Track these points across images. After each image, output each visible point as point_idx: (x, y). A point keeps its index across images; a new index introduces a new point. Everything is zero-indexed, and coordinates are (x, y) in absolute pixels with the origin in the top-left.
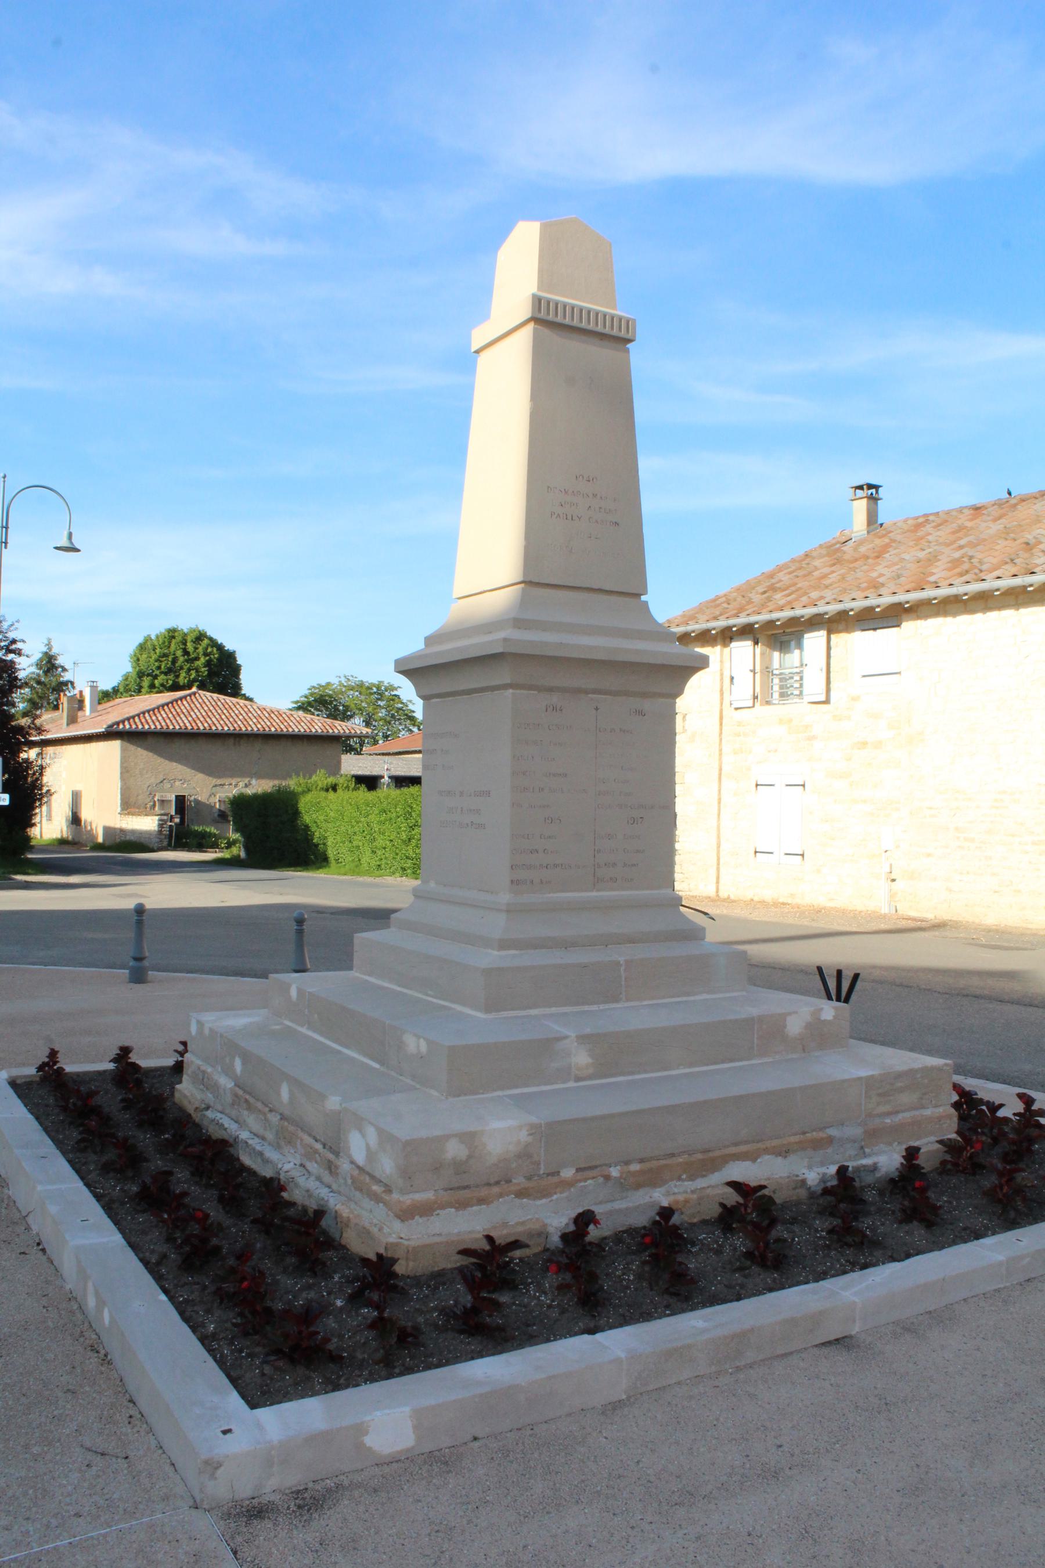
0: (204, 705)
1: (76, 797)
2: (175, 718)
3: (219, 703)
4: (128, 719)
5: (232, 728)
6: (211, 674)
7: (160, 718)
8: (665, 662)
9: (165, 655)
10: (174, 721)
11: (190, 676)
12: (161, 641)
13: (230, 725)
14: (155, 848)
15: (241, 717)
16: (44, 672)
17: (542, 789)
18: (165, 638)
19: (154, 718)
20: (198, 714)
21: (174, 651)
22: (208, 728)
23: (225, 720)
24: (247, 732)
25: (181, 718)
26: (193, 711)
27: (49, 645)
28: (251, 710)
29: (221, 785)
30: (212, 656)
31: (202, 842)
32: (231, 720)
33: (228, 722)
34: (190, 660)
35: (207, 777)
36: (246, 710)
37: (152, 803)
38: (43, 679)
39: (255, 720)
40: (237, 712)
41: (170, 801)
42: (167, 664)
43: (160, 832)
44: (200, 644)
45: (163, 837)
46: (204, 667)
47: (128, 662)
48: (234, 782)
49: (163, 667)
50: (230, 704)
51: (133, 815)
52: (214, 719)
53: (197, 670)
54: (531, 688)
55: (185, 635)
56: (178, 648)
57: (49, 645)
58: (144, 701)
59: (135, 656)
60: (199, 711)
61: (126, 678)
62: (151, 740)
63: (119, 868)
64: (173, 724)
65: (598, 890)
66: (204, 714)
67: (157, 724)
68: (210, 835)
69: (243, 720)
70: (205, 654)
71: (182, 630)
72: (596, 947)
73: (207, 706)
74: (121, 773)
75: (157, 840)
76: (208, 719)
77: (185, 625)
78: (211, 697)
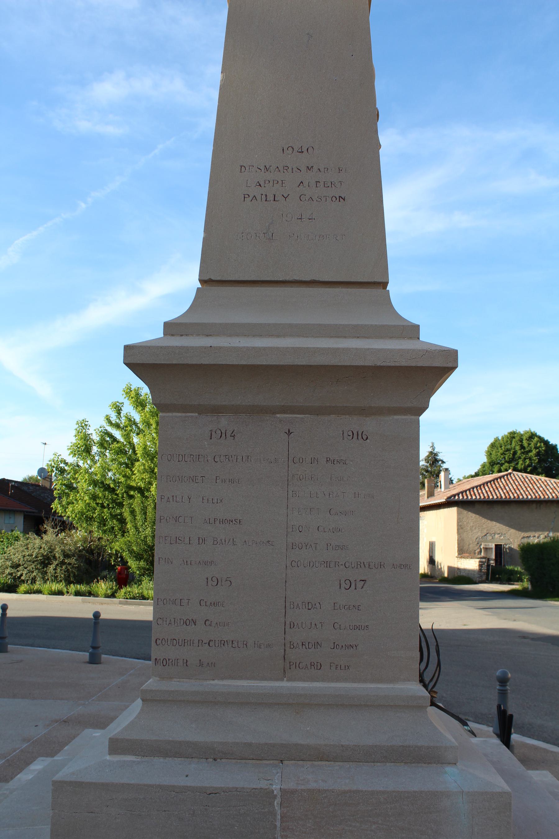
0: (516, 482)
1: (432, 546)
2: (494, 491)
3: (527, 480)
4: (462, 493)
5: (534, 497)
6: (540, 461)
7: (484, 491)
8: (379, 364)
9: (508, 450)
10: (493, 493)
11: (525, 463)
12: (505, 439)
13: (532, 495)
14: (477, 582)
15: (541, 489)
16: (430, 464)
17: (204, 540)
18: (508, 438)
19: (480, 491)
20: (511, 487)
21: (515, 447)
22: (517, 497)
23: (530, 491)
24: (545, 499)
25: (499, 491)
26: (508, 485)
27: (433, 447)
28: (549, 483)
29: (527, 537)
30: (540, 449)
31: (510, 578)
32: (534, 491)
33: (531, 493)
34: (526, 452)
35: (517, 532)
36: (545, 483)
37: (479, 550)
38: (429, 469)
39: (551, 491)
40: (539, 485)
41: (492, 548)
42: (510, 456)
43: (480, 570)
44: (532, 441)
45: (483, 574)
46: (535, 457)
47: (484, 456)
48: (537, 535)
49: (506, 458)
50: (535, 480)
51: (464, 558)
52: (522, 491)
53: (530, 459)
54: (185, 408)
55: (522, 435)
56: (517, 444)
57: (433, 447)
58: (479, 480)
59: (489, 452)
60: (512, 485)
61: (483, 466)
62: (477, 506)
64: (492, 495)
66: (515, 487)
67: (481, 495)
68: (517, 572)
69: (542, 491)
70: (536, 448)
71: (520, 432)
73: (518, 482)
74: (458, 529)
75: (479, 576)
76: (517, 491)
77: (521, 429)
78: (522, 475)
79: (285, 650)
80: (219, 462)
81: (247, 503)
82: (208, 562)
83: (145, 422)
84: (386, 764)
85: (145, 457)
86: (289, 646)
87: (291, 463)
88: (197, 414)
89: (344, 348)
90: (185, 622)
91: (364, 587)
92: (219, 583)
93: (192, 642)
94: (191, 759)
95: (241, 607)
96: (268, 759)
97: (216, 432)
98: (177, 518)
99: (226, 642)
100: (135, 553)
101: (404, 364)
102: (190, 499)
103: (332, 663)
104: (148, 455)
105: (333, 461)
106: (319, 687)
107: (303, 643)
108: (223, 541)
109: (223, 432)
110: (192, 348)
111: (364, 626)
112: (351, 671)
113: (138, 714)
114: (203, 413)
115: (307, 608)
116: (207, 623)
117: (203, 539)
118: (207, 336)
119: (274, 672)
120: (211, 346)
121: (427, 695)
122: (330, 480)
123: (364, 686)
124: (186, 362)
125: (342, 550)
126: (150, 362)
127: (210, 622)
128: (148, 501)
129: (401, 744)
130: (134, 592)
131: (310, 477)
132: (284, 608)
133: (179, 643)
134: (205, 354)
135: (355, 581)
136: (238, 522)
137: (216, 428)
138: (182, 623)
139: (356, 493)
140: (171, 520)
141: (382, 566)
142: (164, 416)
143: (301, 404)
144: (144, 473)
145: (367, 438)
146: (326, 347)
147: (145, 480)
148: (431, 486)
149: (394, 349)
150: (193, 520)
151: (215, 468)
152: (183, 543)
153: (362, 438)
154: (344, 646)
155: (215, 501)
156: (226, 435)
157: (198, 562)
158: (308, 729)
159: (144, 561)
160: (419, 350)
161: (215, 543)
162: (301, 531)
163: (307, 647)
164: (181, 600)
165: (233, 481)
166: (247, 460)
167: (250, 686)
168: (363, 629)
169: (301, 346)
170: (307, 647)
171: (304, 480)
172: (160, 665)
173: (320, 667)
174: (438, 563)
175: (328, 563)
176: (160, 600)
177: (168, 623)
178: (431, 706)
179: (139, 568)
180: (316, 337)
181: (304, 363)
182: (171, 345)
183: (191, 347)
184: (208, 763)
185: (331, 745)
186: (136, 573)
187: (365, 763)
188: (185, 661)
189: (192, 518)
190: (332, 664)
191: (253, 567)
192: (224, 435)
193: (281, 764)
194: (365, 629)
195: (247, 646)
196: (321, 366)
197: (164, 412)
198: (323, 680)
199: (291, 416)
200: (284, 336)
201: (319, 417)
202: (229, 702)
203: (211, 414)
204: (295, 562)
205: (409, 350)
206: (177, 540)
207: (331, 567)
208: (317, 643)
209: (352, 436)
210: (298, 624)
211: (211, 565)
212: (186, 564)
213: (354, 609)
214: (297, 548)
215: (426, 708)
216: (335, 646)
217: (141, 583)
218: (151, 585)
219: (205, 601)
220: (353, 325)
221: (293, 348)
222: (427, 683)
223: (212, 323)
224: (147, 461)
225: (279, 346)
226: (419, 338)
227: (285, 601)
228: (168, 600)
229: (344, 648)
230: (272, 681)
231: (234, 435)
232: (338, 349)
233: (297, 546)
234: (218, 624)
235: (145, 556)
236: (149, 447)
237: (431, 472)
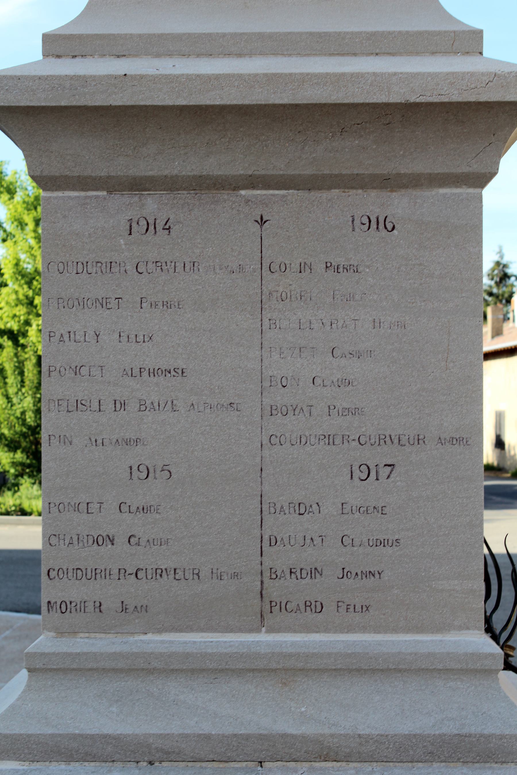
1: (500, 418)
8: (413, 99)
17: (123, 404)
38: (495, 291)
63: (499, 499)
65: (271, 630)
72: (232, 764)
79: (262, 582)
80: (145, 273)
81: (193, 342)
82: (132, 441)
83: (16, 220)
84: (432, 764)
85: (17, 279)
86: (269, 574)
87: (266, 272)
88: (105, 193)
89: (354, 73)
90: (96, 540)
91: (392, 476)
92: (150, 475)
93: (108, 572)
94: (111, 764)
95: (187, 513)
96: (238, 760)
97: (138, 223)
98: (78, 368)
99: (164, 571)
100: (6, 440)
101: (456, 98)
102: (98, 336)
103: (341, 601)
104: (23, 276)
105: (336, 267)
106: (320, 641)
107: (293, 570)
108: (156, 404)
109: (151, 222)
110: (93, 78)
111: (393, 541)
112: (372, 614)
113: (22, 692)
114: (115, 191)
115: (297, 512)
116: (132, 540)
117: (123, 403)
118: (118, 57)
119: (245, 618)
120: (125, 75)
121: (498, 652)
122: (332, 300)
123: (394, 639)
124: (82, 102)
125: (354, 416)
126: (22, 104)
127: (137, 539)
128: (26, 353)
129: (456, 732)
130: (7, 504)
131: (298, 295)
132: (259, 514)
133: (86, 574)
134: (116, 88)
135: (377, 466)
136: (180, 373)
137: (139, 216)
138: (91, 541)
139: (376, 320)
140: (67, 372)
141: (421, 442)
142: (50, 197)
143: (281, 172)
144: (17, 305)
145: (393, 228)
146: (322, 71)
147: (19, 317)
148: (498, 319)
149: (440, 73)
150: (104, 371)
151: (139, 283)
152: (89, 409)
153: (386, 227)
154: (359, 574)
155: (140, 338)
156: (155, 228)
157: (115, 440)
158: (303, 709)
159: (22, 452)
160: (483, 74)
161: (142, 409)
162: (284, 384)
163: (299, 577)
164: (88, 503)
165: (169, 305)
166: (192, 268)
167: (205, 642)
168: (390, 544)
169: (279, 71)
170: (299, 577)
171: (288, 300)
172: (56, 612)
173: (320, 608)
174: (509, 446)
175: (331, 437)
176: (52, 505)
177: (67, 542)
178: (504, 669)
179: (14, 464)
180: (305, 55)
181: (285, 101)
182: (57, 74)
183: (91, 76)
184: (140, 769)
185: (341, 735)
186: (8, 472)
187: (397, 764)
188: (98, 604)
189: (103, 368)
190: (340, 604)
191: (207, 446)
192: (151, 228)
193: (259, 768)
194: (394, 545)
195: (199, 577)
196: (315, 105)
197: (49, 190)
198: (327, 630)
199: (264, 192)
200: (251, 54)
201: (312, 193)
202: (172, 670)
203: (130, 193)
204: (276, 437)
205: (464, 73)
206: (79, 405)
207: (335, 443)
208: (316, 569)
209: (368, 224)
210: (282, 539)
211: (137, 445)
212: (94, 444)
213: (376, 513)
214: (279, 414)
215: (497, 674)
216: (345, 574)
217: (19, 489)
218: (35, 490)
219: (128, 505)
220: (368, 33)
221: (265, 75)
222: (498, 632)
223: (126, 34)
224: (20, 286)
225: (241, 72)
226: (481, 53)
227: (261, 501)
228: (66, 504)
229: (360, 577)
230: (242, 632)
231: (170, 227)
232: (343, 74)
233: (279, 410)
234: (151, 541)
235: (24, 444)
236: (24, 262)
237: (497, 296)
